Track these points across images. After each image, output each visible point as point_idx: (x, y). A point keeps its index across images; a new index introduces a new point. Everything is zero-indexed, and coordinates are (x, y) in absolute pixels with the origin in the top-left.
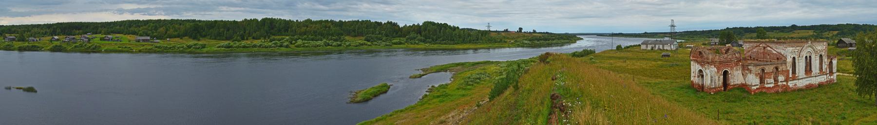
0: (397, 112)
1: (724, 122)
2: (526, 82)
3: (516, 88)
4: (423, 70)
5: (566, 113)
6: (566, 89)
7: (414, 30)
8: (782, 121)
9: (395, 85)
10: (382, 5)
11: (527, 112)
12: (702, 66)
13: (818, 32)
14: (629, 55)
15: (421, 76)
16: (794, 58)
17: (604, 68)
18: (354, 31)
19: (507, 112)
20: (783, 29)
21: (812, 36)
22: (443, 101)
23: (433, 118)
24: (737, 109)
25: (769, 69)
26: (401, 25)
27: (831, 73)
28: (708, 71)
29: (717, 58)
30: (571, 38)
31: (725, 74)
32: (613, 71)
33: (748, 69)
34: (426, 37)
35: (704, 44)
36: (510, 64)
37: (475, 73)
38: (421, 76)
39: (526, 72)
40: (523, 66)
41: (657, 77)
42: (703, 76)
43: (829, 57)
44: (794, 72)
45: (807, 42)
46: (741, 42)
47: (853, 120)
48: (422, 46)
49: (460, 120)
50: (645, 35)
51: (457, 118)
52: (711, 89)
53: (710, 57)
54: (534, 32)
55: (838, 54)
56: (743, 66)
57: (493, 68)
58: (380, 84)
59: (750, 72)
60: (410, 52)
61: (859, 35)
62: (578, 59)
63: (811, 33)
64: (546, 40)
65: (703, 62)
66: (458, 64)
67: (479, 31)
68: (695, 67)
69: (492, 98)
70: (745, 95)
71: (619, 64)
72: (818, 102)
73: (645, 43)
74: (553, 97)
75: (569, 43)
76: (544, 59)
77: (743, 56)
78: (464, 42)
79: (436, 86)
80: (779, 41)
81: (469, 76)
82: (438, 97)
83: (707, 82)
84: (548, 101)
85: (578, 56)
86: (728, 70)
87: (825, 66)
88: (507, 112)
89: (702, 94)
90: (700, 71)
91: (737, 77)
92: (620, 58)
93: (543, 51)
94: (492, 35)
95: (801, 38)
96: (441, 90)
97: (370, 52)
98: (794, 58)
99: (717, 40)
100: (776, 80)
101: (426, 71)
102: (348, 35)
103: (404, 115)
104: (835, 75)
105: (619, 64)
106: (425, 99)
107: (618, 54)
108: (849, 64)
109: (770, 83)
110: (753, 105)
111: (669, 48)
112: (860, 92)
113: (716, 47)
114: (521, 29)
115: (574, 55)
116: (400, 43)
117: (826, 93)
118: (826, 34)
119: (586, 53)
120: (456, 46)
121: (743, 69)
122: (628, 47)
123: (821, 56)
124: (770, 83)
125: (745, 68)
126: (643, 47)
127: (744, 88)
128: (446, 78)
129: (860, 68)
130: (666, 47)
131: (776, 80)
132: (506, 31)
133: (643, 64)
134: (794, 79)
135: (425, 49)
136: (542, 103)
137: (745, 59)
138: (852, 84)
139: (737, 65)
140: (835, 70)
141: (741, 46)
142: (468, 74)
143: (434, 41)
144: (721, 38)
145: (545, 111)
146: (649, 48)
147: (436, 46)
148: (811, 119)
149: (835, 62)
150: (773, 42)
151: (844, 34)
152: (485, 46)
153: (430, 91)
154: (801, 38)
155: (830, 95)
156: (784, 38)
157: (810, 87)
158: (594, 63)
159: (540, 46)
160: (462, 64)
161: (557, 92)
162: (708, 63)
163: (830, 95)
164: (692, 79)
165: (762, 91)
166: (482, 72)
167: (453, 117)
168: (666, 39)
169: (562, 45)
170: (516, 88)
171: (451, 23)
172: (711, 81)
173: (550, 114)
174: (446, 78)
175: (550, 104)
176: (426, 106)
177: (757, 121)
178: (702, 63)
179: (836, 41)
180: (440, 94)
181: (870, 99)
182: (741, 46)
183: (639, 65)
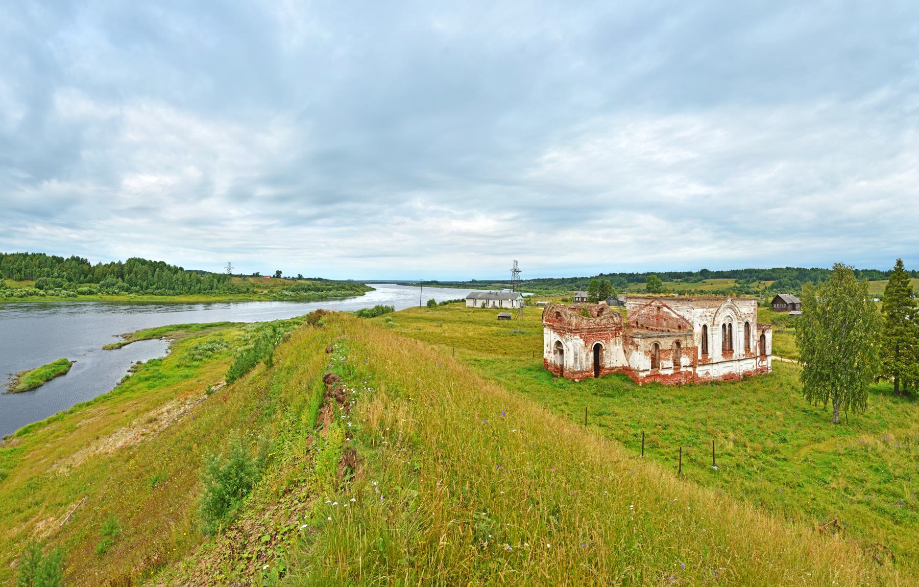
0: (80, 406)
1: (595, 428)
2: (286, 355)
3: (270, 364)
4: (125, 336)
5: (346, 405)
6: (348, 368)
7: (112, 272)
8: (687, 435)
9: (80, 361)
10: (66, 230)
11: (285, 403)
12: (560, 334)
13: (743, 281)
14: (448, 315)
15: (120, 346)
16: (705, 327)
17: (406, 335)
18: (19, 271)
19: (255, 403)
20: (686, 277)
21: (733, 289)
22: (155, 386)
23: (137, 413)
24: (616, 409)
25: (666, 343)
26: (93, 264)
27: (763, 355)
28: (570, 344)
29: (584, 324)
30: (356, 288)
31: (597, 349)
32: (422, 340)
33: (633, 343)
34: (131, 283)
35: (565, 300)
36: (261, 327)
37: (204, 341)
38: (120, 346)
39: (286, 339)
40: (282, 330)
41: (490, 351)
42: (562, 352)
43: (759, 326)
44: (705, 352)
45: (725, 299)
46: (621, 298)
47: (799, 446)
48: (125, 297)
49: (179, 417)
50: (473, 284)
51: (175, 413)
52: (575, 373)
53: (574, 321)
54: (300, 277)
55: (774, 323)
56: (625, 336)
57: (235, 333)
58: (57, 360)
59: (637, 347)
60: (105, 308)
61: (805, 287)
62: (367, 321)
63: (731, 283)
64: (318, 290)
65: (562, 329)
66: (179, 327)
67: (214, 275)
68: (550, 337)
69: (231, 380)
70: (628, 385)
71: (430, 328)
72: (743, 406)
73: (474, 298)
74: (327, 380)
75: (354, 296)
76: (314, 319)
77: (625, 321)
78: (190, 292)
79: (144, 361)
80: (683, 297)
81: (197, 348)
82: (147, 379)
83: (569, 362)
84: (318, 386)
85: (367, 316)
86: (602, 342)
87: (754, 343)
88: (255, 403)
89: (561, 381)
90: (559, 343)
91: (615, 355)
92: (432, 320)
93: (313, 307)
94: (235, 281)
95: (716, 293)
96: (152, 369)
97: (44, 307)
98: (705, 327)
99: (585, 294)
100: (677, 364)
101: (129, 338)
102: (9, 277)
103: (91, 410)
104: (770, 359)
105: (430, 328)
106: (127, 384)
107: (430, 314)
108: (791, 342)
109: (667, 367)
110: (640, 403)
111: (509, 306)
112: (809, 393)
113: (583, 305)
114: (279, 273)
115: (361, 314)
116: (91, 293)
117: (755, 391)
118: (754, 286)
119: (381, 311)
120: (177, 299)
121: (626, 343)
122: (445, 303)
123: (747, 324)
124: (667, 367)
125: (628, 341)
126: (469, 303)
127: (626, 373)
128: (159, 349)
129: (809, 352)
130: (506, 304)
131: (677, 364)
132: (256, 275)
133: (472, 331)
134: (705, 362)
135: (129, 303)
136: (309, 389)
137: (628, 326)
138: (796, 379)
139: (615, 335)
140: (768, 351)
141: (622, 304)
142: (195, 343)
143: (144, 290)
144: (591, 290)
145: (314, 402)
146: (479, 304)
147: (145, 298)
148: (732, 436)
149: (769, 336)
150: (673, 299)
151: (781, 286)
152: (223, 298)
153: (134, 370)
154: (716, 293)
155: (762, 395)
156: (690, 292)
157: (729, 379)
158: (392, 326)
159: (308, 300)
160: (187, 327)
161: (333, 372)
162: (571, 331)
163: (762, 395)
164: (545, 355)
165: (655, 381)
166: (217, 339)
167: (168, 412)
168: (506, 291)
169: (343, 298)
170: (270, 364)
171: (171, 262)
172: (576, 359)
173: (321, 406)
174: (159, 349)
175: (321, 391)
176: (128, 394)
177: (647, 432)
178: (561, 331)
179: (771, 299)
180: (149, 374)
181: (825, 409)
182: (622, 304)
183: (459, 331)
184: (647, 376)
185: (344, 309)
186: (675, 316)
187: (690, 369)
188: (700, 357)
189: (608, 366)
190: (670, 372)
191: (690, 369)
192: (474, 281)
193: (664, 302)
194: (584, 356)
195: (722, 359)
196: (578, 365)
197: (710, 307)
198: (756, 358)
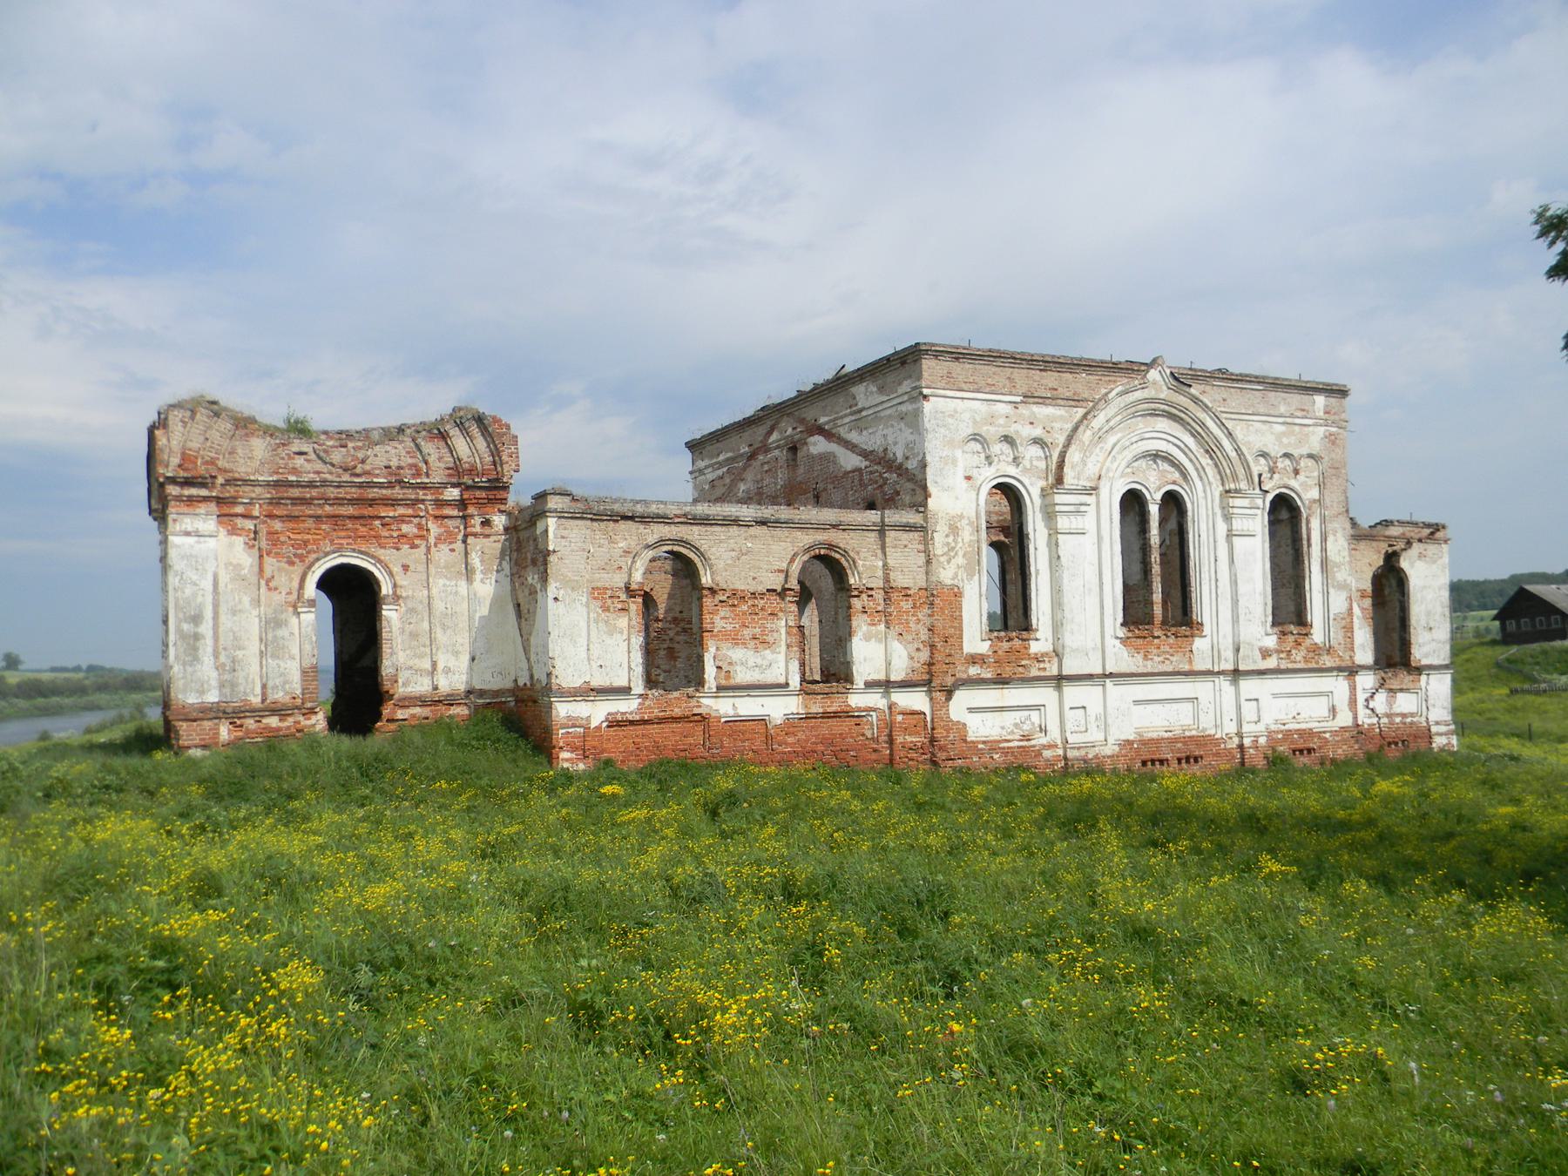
27: (1394, 654)
31: (354, 598)
44: (1013, 613)
124: (755, 679)
184: (615, 723)
185: (1443, 632)
186: (849, 461)
187: (916, 700)
188: (975, 638)
189: (422, 686)
190: (779, 709)
191: (916, 700)
193: (810, 413)
194: (251, 626)
196: (207, 669)
197: (1029, 397)
198: (1352, 671)
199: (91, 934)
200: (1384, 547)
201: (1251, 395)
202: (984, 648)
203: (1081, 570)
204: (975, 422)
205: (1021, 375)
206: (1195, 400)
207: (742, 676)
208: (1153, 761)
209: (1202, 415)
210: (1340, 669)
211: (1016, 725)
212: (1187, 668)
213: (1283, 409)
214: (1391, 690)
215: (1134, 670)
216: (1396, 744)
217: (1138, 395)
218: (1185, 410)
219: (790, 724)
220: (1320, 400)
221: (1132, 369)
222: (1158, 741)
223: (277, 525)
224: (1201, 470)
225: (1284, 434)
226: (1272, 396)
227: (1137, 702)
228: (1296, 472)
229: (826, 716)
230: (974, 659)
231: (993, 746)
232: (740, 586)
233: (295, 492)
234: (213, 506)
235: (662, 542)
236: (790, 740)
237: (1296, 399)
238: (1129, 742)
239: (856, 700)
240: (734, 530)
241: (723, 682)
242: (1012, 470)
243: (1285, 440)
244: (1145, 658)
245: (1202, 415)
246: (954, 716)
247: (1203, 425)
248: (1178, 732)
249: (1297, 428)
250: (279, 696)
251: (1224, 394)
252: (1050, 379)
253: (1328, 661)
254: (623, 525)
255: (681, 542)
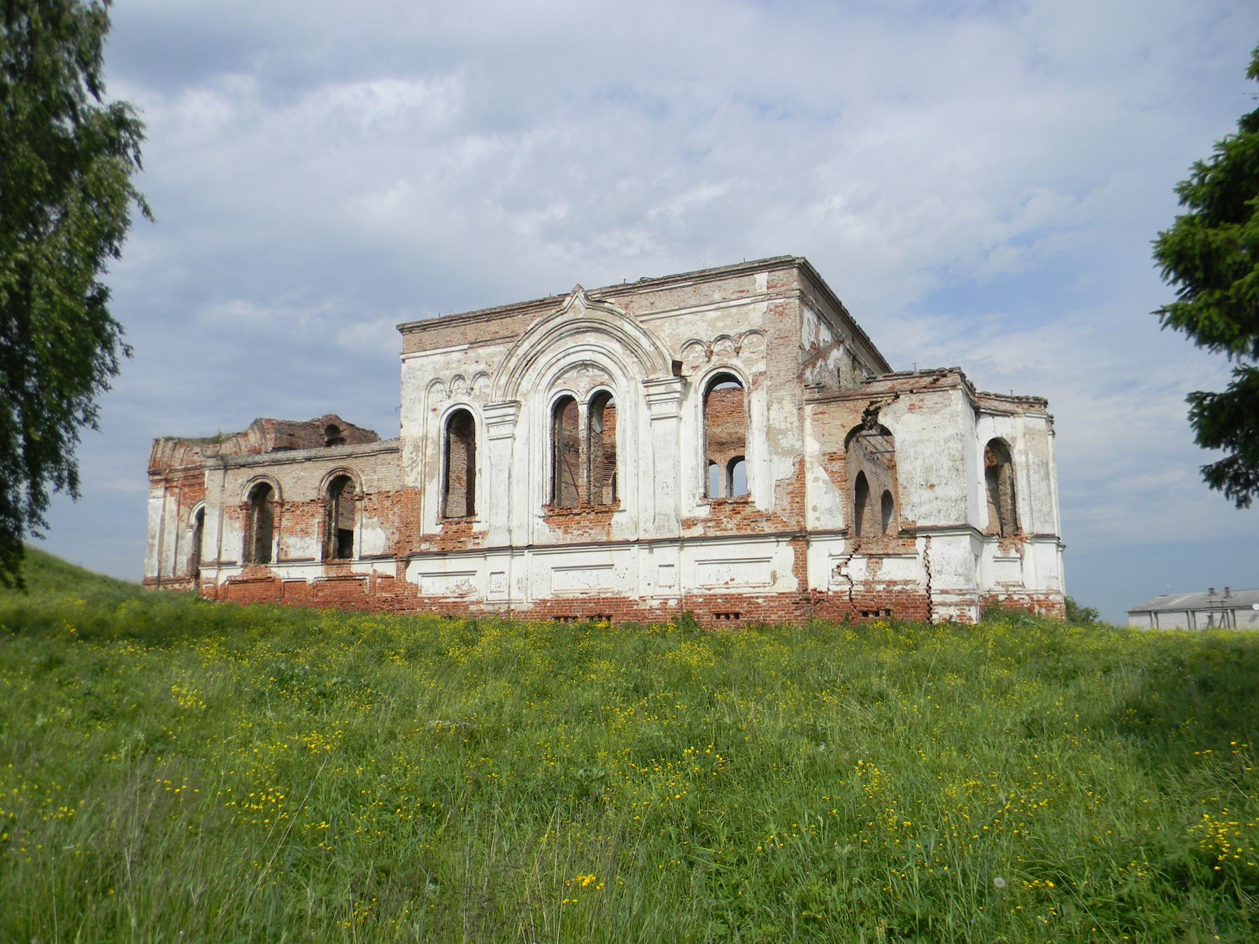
27: (1007, 528)
100: (340, 545)
124: (300, 557)
184: (233, 582)
187: (389, 568)
188: (430, 524)
190: (313, 574)
191: (389, 568)
192: (643, 280)
195: (545, 534)
196: (155, 562)
197: (474, 344)
198: (801, 537)
199: (405, 741)
200: (863, 405)
201: (680, 292)
202: (437, 530)
203: (515, 463)
204: (435, 370)
205: (472, 331)
206: (611, 312)
207: (293, 554)
208: (566, 618)
209: (618, 323)
210: (779, 535)
211: (457, 586)
212: (604, 539)
213: (717, 297)
214: (871, 556)
215: (554, 542)
216: (877, 614)
217: (559, 320)
218: (603, 322)
219: (317, 586)
220: (762, 278)
221: (553, 303)
222: (570, 602)
223: (186, 490)
224: (623, 369)
225: (718, 319)
226: (705, 287)
227: (557, 569)
228: (738, 351)
229: (340, 579)
230: (428, 539)
231: (434, 600)
232: (296, 500)
233: (192, 473)
234: (163, 484)
235: (255, 478)
236: (320, 594)
237: (732, 284)
238: (545, 601)
239: (357, 568)
240: (295, 466)
241: (283, 558)
242: (465, 399)
243: (720, 324)
244: (566, 532)
245: (618, 323)
246: (409, 579)
247: (622, 331)
248: (593, 593)
249: (734, 310)
250: (179, 573)
251: (652, 298)
252: (494, 326)
253: (768, 528)
254: (243, 470)
255: (264, 476)
